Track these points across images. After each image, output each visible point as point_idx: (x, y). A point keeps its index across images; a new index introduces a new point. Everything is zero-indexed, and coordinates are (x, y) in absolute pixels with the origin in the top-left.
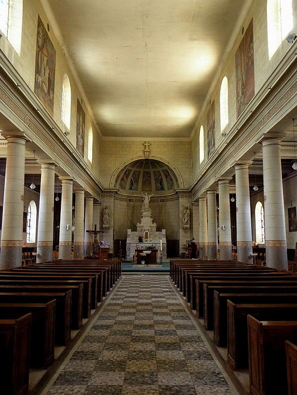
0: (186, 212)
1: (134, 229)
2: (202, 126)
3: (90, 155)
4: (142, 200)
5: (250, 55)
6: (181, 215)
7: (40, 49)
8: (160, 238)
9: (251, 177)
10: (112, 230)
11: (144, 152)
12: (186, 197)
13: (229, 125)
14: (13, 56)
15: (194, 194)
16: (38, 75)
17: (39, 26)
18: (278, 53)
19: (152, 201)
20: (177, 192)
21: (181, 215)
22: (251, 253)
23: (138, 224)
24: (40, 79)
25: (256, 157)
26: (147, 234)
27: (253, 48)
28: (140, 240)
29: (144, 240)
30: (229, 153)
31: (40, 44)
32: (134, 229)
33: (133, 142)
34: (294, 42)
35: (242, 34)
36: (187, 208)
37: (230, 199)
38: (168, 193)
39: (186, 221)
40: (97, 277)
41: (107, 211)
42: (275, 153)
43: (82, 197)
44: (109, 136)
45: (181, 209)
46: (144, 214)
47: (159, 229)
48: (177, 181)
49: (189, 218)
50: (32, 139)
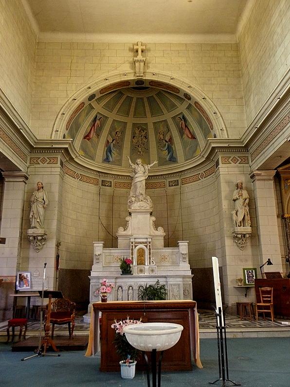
1: (111, 242)
4: (128, 182)
6: (225, 204)
8: (175, 264)
10: (52, 245)
12: (235, 160)
20: (214, 148)
21: (225, 204)
23: (121, 231)
26: (141, 253)
28: (126, 268)
29: (134, 266)
32: (111, 242)
33: (109, 45)
36: (239, 187)
39: (240, 218)
41: (40, 195)
44: (54, 30)
45: (224, 189)
46: (136, 206)
47: (171, 242)
49: (247, 208)
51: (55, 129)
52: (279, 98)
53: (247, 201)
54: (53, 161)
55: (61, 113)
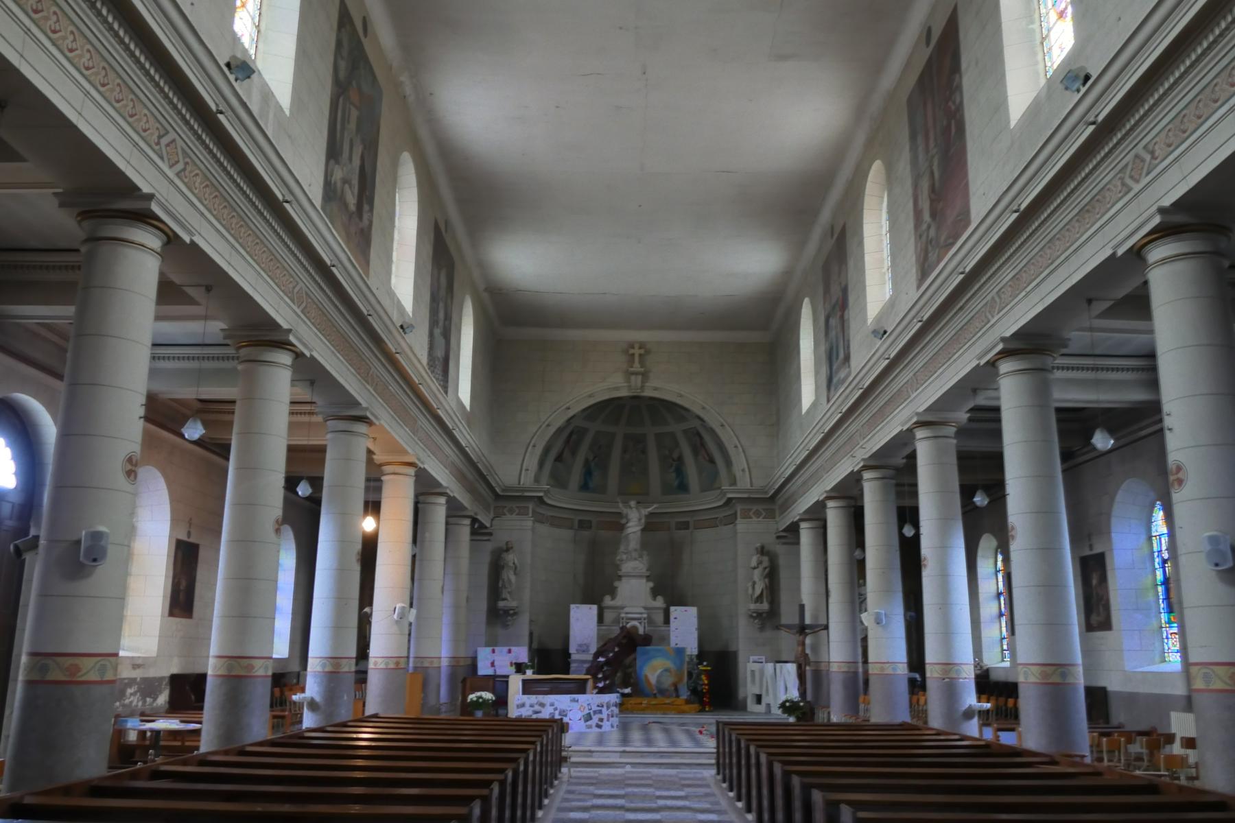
0: (760, 563)
2: (806, 301)
3: (464, 390)
4: (617, 524)
5: (953, 108)
7: (341, 89)
9: (965, 460)
11: (629, 374)
12: (758, 514)
13: (892, 304)
14: (271, 116)
15: (785, 507)
16: (332, 162)
17: (341, 25)
18: (1035, 110)
19: (649, 527)
20: (730, 500)
22: (970, 699)
24: (338, 174)
25: (981, 400)
27: (959, 88)
30: (895, 387)
31: (342, 74)
34: (1083, 90)
35: (928, 44)
37: (901, 528)
38: (700, 501)
39: (758, 592)
40: (510, 774)
42: (1041, 392)
43: (439, 513)
48: (729, 463)
50: (310, 350)
51: (524, 467)
52: (1093, 123)
53: (767, 570)
54: (523, 512)
55: (531, 444)
